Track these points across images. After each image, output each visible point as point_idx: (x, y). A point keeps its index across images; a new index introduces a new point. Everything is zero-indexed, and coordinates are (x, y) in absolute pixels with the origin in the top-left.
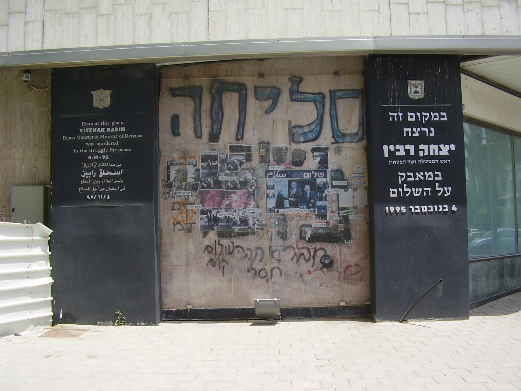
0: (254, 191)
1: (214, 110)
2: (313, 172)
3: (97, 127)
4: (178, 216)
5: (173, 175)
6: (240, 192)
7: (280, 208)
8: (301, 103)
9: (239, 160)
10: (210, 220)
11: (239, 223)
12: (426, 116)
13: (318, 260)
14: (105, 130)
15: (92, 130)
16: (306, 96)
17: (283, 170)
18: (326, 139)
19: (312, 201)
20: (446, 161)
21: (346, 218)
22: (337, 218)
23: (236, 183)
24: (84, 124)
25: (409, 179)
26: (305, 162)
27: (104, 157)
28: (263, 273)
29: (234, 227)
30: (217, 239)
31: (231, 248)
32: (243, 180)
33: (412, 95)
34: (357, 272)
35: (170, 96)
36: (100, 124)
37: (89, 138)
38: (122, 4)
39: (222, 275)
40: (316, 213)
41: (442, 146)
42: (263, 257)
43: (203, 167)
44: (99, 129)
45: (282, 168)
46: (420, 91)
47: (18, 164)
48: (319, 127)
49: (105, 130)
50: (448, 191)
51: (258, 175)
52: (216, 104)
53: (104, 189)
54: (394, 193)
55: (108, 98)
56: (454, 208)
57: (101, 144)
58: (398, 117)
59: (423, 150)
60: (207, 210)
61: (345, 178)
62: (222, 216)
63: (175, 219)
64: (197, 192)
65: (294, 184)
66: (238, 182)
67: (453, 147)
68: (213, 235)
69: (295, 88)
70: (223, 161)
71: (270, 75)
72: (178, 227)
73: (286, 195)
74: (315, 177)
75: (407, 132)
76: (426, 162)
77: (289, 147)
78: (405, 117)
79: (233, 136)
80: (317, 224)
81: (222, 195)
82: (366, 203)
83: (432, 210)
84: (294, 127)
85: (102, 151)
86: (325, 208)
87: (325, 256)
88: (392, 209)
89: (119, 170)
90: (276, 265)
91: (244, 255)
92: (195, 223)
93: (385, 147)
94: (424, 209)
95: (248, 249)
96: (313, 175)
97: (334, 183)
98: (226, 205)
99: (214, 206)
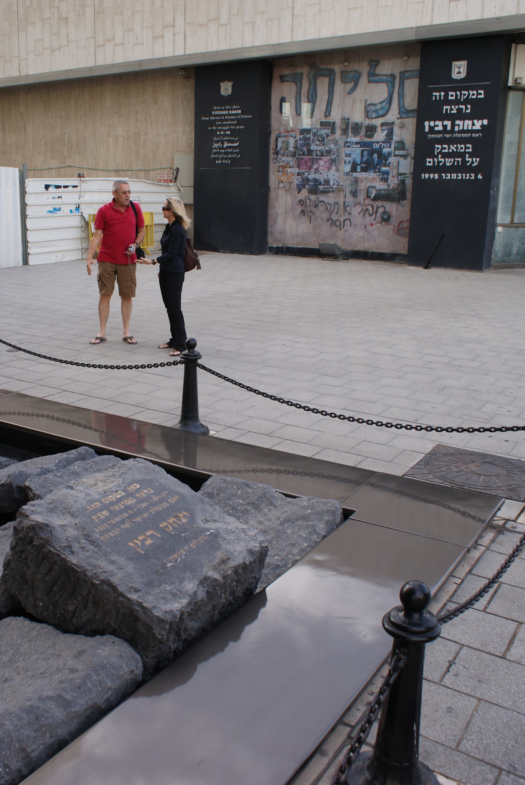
0: (335, 158)
2: (381, 143)
3: (223, 110)
5: (280, 145)
6: (326, 159)
8: (376, 84)
9: (326, 134)
10: (303, 181)
11: (323, 183)
12: (465, 95)
13: (379, 215)
14: (229, 112)
18: (393, 115)
19: (378, 167)
20: (477, 135)
23: (323, 152)
24: (215, 108)
25: (443, 151)
27: (227, 132)
28: (338, 223)
29: (319, 186)
30: (307, 195)
31: (317, 202)
33: (455, 76)
37: (218, 118)
38: (235, 15)
40: (380, 177)
41: (475, 121)
42: (338, 211)
43: (300, 139)
45: (357, 139)
46: (462, 72)
47: (180, 136)
48: (388, 105)
49: (229, 112)
50: (476, 161)
52: (312, 88)
54: (430, 162)
55: (230, 88)
56: (480, 177)
58: (440, 96)
59: (459, 125)
61: (406, 148)
63: (279, 179)
65: (365, 153)
66: (324, 151)
68: (304, 192)
69: (372, 71)
70: (315, 134)
72: (281, 185)
73: (358, 162)
75: (447, 110)
76: (460, 135)
77: (364, 122)
78: (446, 96)
79: (323, 114)
80: (381, 186)
81: (313, 161)
83: (460, 178)
84: (369, 105)
85: (226, 128)
86: (387, 173)
87: (385, 212)
88: (427, 176)
89: (237, 142)
90: (347, 217)
91: (325, 208)
92: (292, 182)
93: (426, 123)
95: (329, 204)
96: (380, 146)
97: (397, 153)
98: (315, 169)
99: (306, 169)
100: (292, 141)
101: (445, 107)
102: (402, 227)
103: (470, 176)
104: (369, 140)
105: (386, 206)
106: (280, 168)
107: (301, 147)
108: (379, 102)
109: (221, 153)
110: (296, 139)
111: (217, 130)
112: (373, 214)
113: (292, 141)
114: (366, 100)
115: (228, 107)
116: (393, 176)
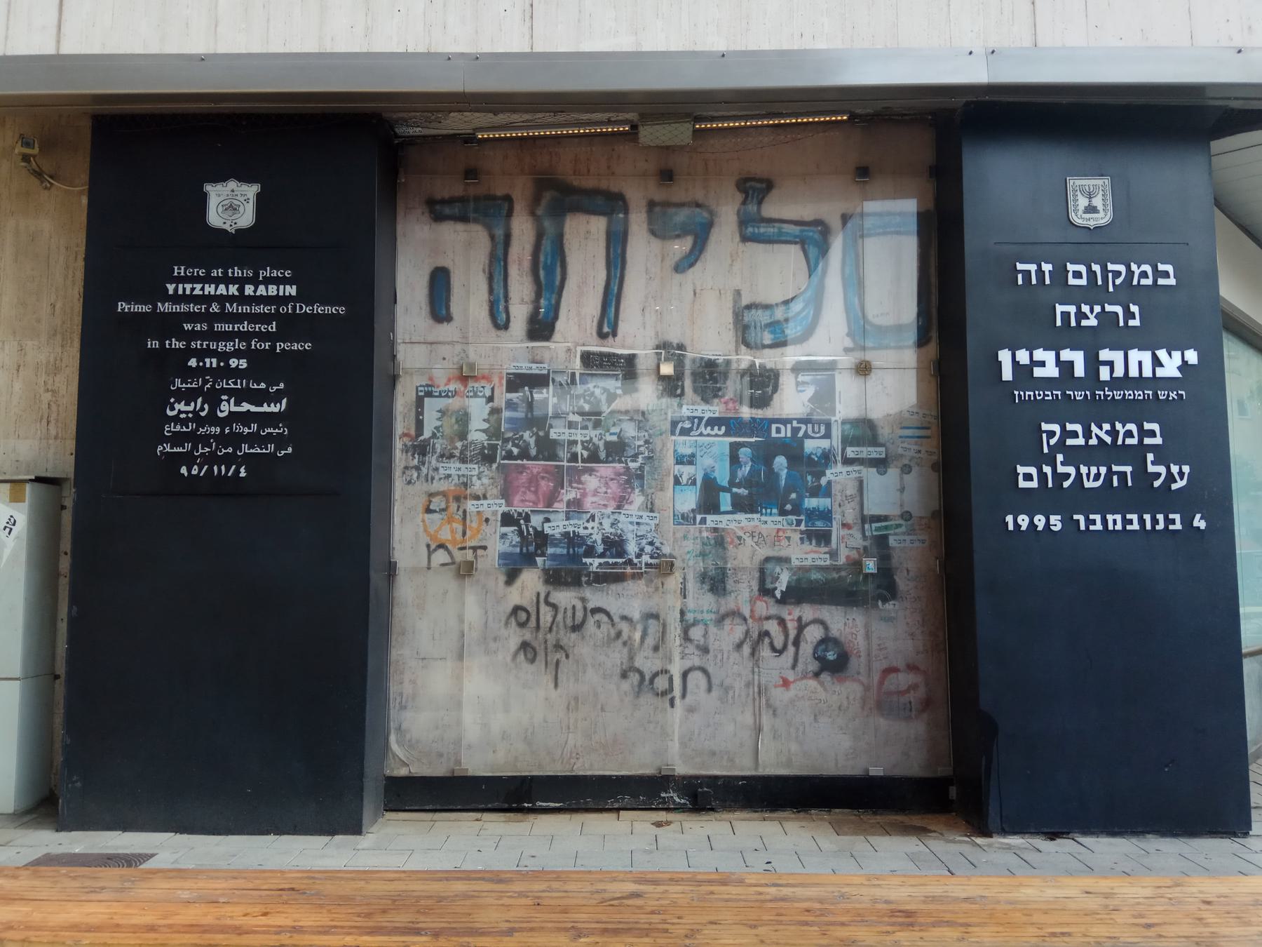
0: (641, 468)
1: (542, 258)
3: (217, 281)
4: (440, 528)
6: (605, 470)
7: (709, 513)
9: (605, 390)
12: (1117, 274)
14: (241, 290)
15: (203, 289)
16: (780, 229)
17: (717, 415)
19: (793, 496)
20: (1173, 395)
21: (881, 541)
22: (857, 540)
23: (597, 448)
24: (179, 271)
25: (1070, 442)
26: (775, 396)
27: (233, 363)
28: (661, 683)
29: (588, 561)
30: (543, 589)
31: (580, 614)
32: (614, 438)
33: (1079, 218)
34: (914, 687)
35: (426, 218)
36: (225, 273)
39: (552, 685)
40: (803, 527)
43: (510, 405)
44: (222, 287)
45: (715, 409)
46: (1100, 207)
49: (241, 290)
51: (654, 427)
53: (230, 450)
56: (184, 470)
57: (228, 327)
58: (1040, 272)
59: (1111, 364)
60: (520, 514)
61: (881, 440)
62: (557, 531)
63: (433, 537)
64: (494, 466)
65: (744, 453)
66: (601, 444)
67: (1192, 356)
68: (531, 580)
71: (689, 174)
72: (440, 557)
74: (801, 434)
76: (1118, 395)
77: (734, 357)
78: (1060, 273)
79: (592, 328)
80: (804, 555)
82: (935, 505)
84: (749, 307)
86: (826, 515)
87: (827, 641)
88: (1024, 521)
89: (276, 398)
90: (696, 661)
91: (613, 633)
92: (485, 548)
93: (1005, 356)
94: (1115, 521)
95: (624, 618)
96: (795, 431)
97: (851, 452)
98: (569, 503)
99: (535, 503)
100: (478, 411)
101: (1060, 309)
102: (893, 688)
103: (1169, 522)
104: (759, 413)
105: (605, 606)
106: (435, 500)
107: (516, 431)
108: (780, 299)
109: (205, 440)
110: (496, 404)
111: (189, 353)
112: (785, 647)
113: (478, 411)
114: (738, 293)
115: (238, 272)
116: (845, 525)
